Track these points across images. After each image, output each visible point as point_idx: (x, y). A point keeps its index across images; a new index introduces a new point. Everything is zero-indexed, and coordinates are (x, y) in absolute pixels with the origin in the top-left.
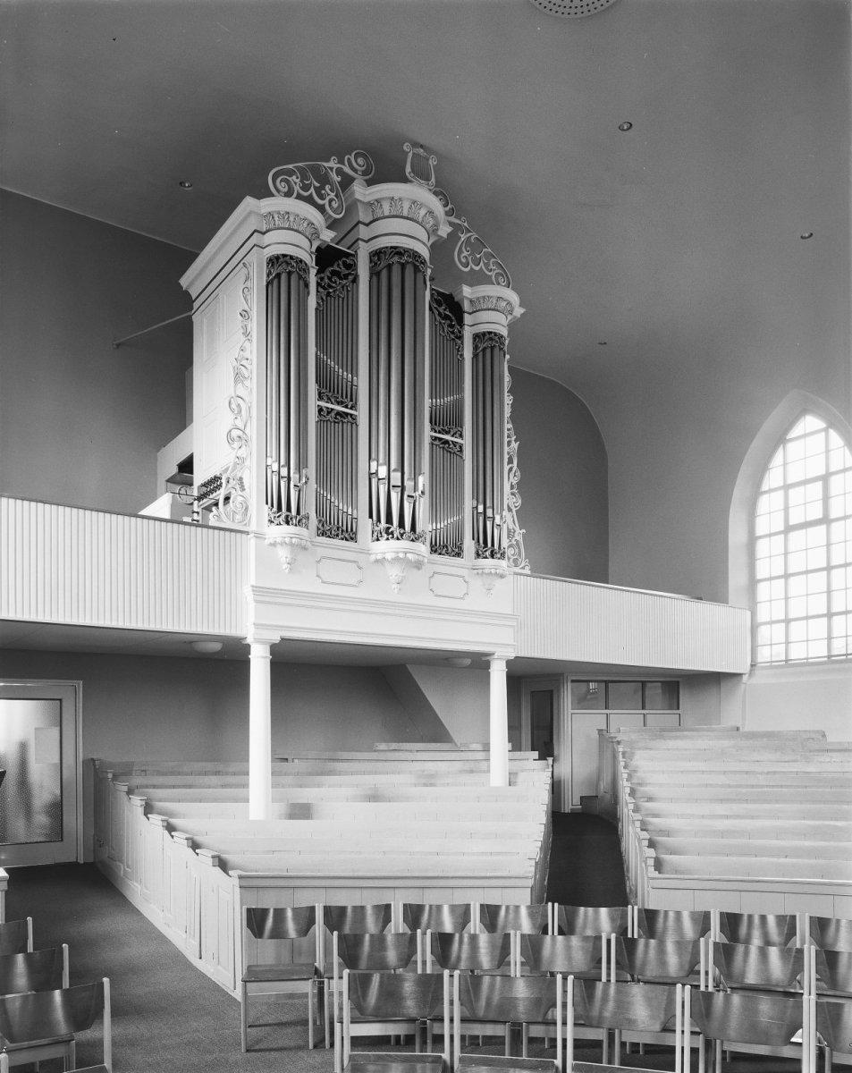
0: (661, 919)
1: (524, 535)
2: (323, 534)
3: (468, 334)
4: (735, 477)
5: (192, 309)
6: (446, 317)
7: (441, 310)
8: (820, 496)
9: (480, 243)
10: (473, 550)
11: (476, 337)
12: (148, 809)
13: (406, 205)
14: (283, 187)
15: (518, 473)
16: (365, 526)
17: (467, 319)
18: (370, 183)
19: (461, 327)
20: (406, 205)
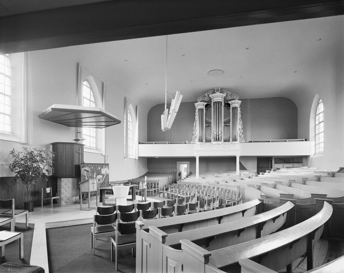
0: (235, 172)
1: (244, 136)
2: (206, 142)
3: (231, 108)
4: (310, 117)
5: (118, 230)
6: (227, 107)
7: (226, 106)
8: (86, 136)
9: (232, 94)
10: (231, 141)
11: (232, 108)
12: (183, 180)
13: (216, 96)
14: (199, 100)
15: (242, 126)
16: (212, 140)
17: (231, 106)
18: (212, 94)
19: (230, 107)
20: (216, 96)
